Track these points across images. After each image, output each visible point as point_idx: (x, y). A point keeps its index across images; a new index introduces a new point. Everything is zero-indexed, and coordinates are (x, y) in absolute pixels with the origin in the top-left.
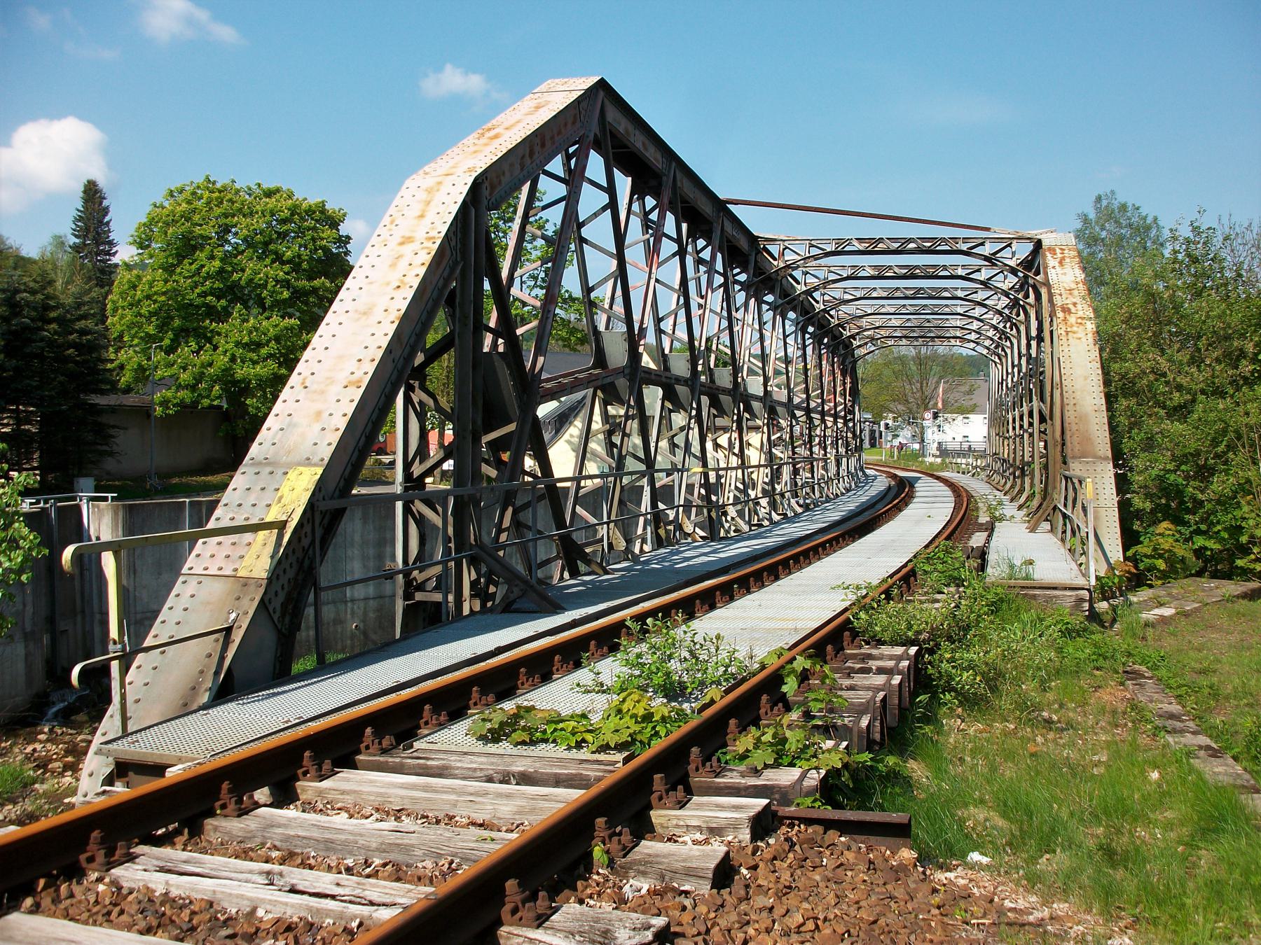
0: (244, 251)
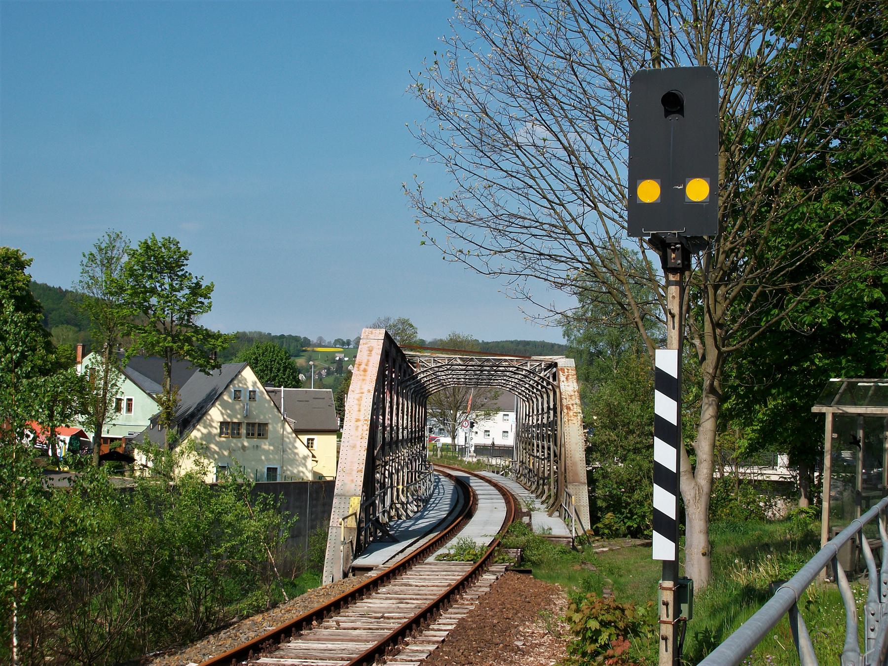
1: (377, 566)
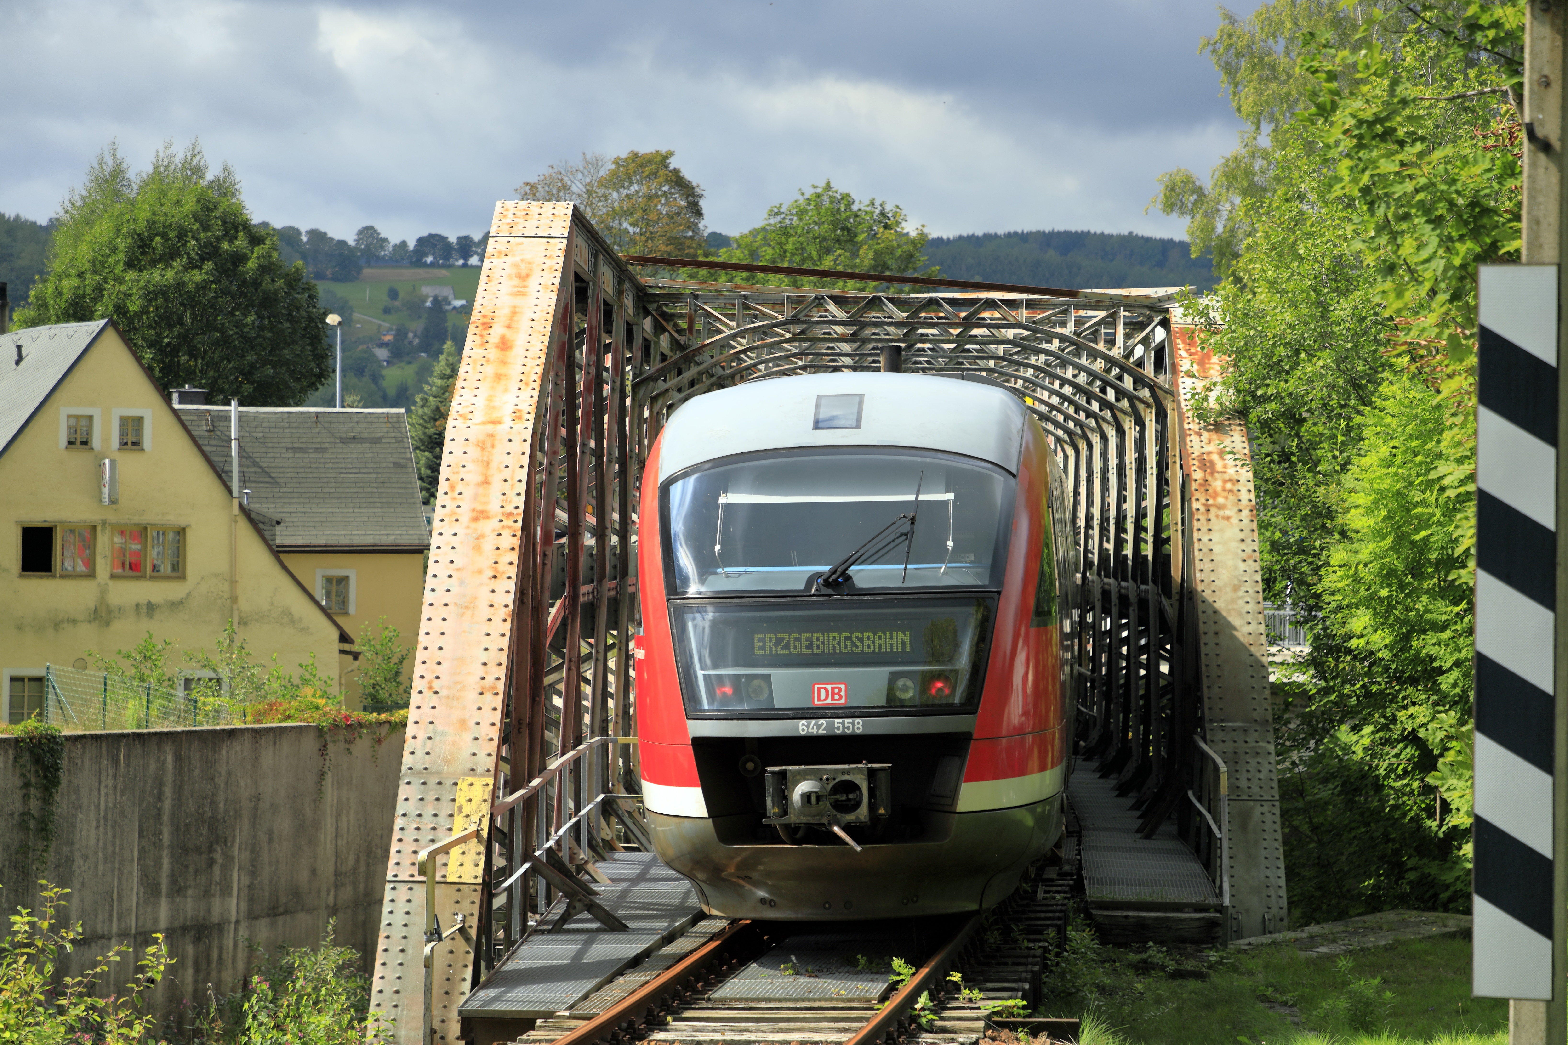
0: (1420, 726)
1: (548, 1015)
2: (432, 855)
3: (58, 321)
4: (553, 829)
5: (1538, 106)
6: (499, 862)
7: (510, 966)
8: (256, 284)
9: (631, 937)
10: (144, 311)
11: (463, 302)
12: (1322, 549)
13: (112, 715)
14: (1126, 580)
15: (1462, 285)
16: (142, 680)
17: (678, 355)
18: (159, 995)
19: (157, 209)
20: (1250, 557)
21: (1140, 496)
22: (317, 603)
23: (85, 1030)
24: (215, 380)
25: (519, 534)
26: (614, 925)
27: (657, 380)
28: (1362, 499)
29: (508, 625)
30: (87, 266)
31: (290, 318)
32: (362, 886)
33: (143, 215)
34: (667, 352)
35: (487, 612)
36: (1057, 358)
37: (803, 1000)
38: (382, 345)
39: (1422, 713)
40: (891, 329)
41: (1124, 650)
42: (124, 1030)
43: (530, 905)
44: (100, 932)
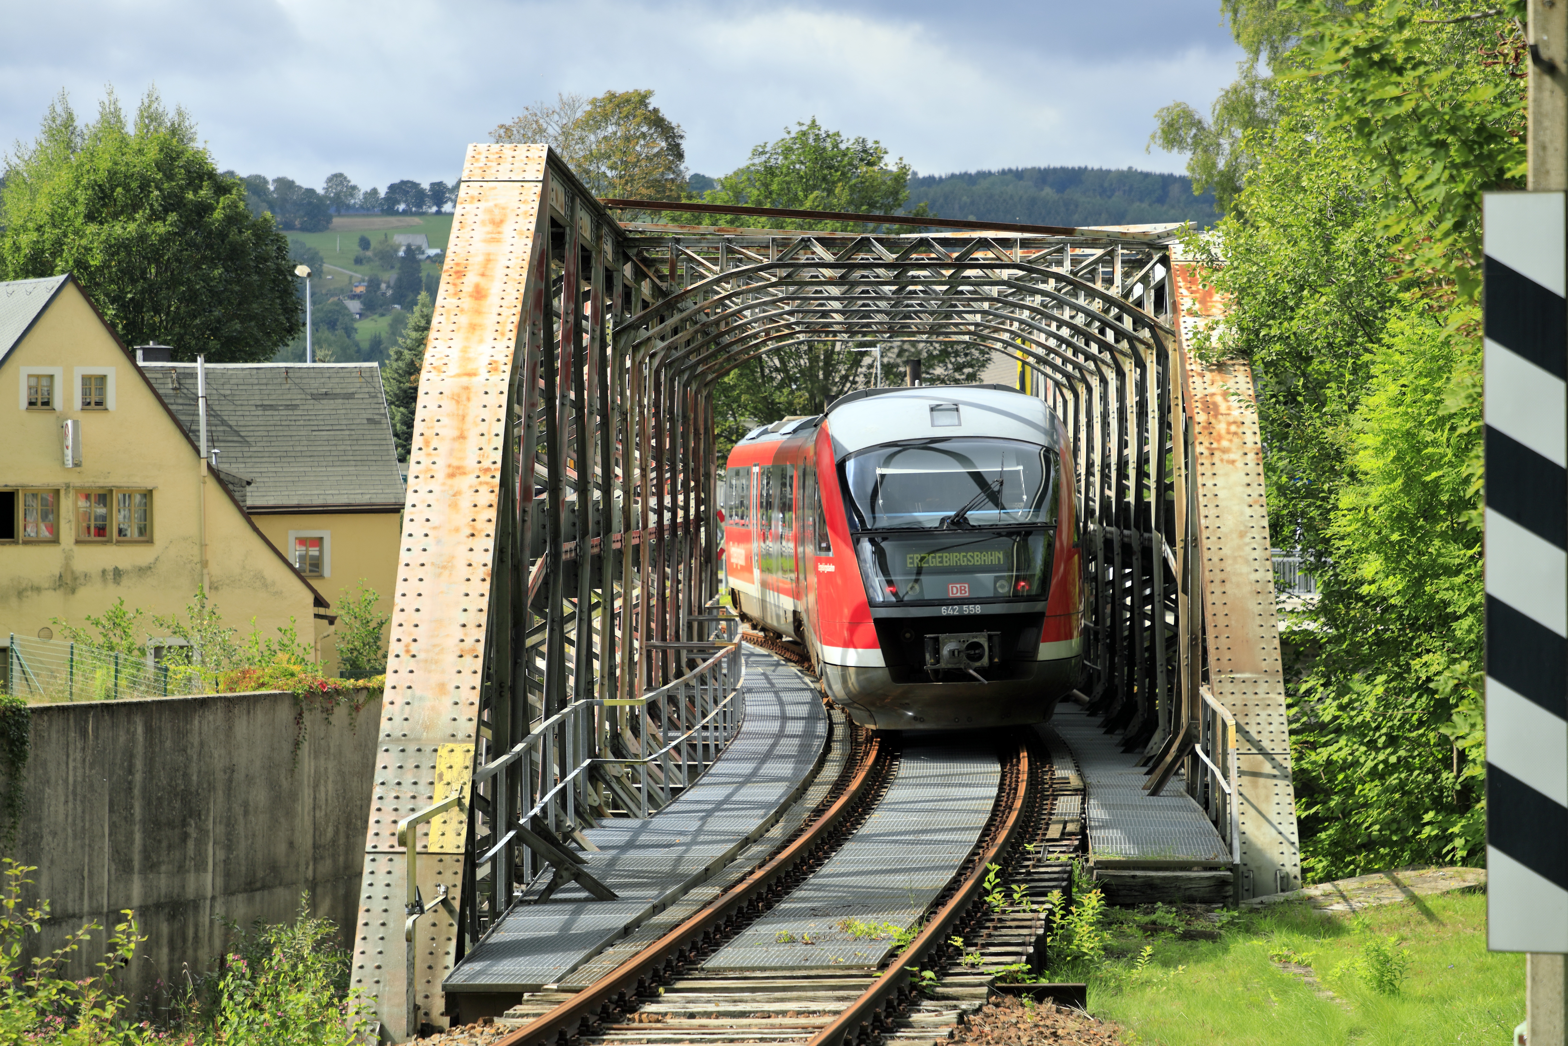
1: (536, 988)
2: (412, 825)
3: (16, 278)
4: (538, 796)
5: (1543, 27)
6: (482, 831)
7: (497, 938)
8: (222, 235)
9: (620, 906)
10: (106, 265)
11: (438, 251)
12: (1330, 491)
13: (79, 685)
14: (1129, 528)
15: (1466, 214)
16: (111, 648)
17: (660, 301)
18: (133, 974)
19: (119, 158)
20: (1256, 502)
21: (1142, 441)
22: (290, 566)
23: (56, 1014)
24: (181, 337)
25: (497, 490)
26: (602, 894)
27: (639, 328)
28: (1370, 440)
29: (487, 585)
30: (46, 218)
31: (259, 272)
32: (341, 859)
33: (104, 164)
34: (648, 299)
35: (466, 572)
36: (1054, 299)
37: (799, 968)
38: (354, 297)
39: (1437, 660)
40: (881, 271)
41: (1128, 601)
42: (96, 1011)
43: (515, 874)
44: (70, 911)
